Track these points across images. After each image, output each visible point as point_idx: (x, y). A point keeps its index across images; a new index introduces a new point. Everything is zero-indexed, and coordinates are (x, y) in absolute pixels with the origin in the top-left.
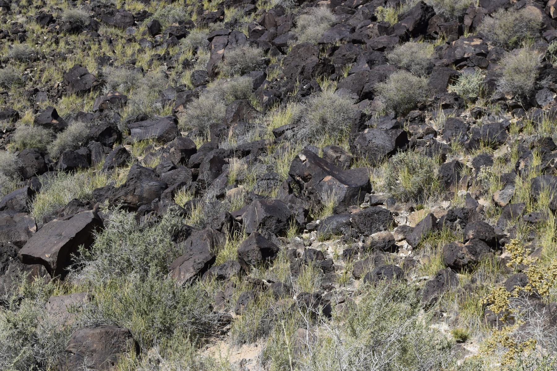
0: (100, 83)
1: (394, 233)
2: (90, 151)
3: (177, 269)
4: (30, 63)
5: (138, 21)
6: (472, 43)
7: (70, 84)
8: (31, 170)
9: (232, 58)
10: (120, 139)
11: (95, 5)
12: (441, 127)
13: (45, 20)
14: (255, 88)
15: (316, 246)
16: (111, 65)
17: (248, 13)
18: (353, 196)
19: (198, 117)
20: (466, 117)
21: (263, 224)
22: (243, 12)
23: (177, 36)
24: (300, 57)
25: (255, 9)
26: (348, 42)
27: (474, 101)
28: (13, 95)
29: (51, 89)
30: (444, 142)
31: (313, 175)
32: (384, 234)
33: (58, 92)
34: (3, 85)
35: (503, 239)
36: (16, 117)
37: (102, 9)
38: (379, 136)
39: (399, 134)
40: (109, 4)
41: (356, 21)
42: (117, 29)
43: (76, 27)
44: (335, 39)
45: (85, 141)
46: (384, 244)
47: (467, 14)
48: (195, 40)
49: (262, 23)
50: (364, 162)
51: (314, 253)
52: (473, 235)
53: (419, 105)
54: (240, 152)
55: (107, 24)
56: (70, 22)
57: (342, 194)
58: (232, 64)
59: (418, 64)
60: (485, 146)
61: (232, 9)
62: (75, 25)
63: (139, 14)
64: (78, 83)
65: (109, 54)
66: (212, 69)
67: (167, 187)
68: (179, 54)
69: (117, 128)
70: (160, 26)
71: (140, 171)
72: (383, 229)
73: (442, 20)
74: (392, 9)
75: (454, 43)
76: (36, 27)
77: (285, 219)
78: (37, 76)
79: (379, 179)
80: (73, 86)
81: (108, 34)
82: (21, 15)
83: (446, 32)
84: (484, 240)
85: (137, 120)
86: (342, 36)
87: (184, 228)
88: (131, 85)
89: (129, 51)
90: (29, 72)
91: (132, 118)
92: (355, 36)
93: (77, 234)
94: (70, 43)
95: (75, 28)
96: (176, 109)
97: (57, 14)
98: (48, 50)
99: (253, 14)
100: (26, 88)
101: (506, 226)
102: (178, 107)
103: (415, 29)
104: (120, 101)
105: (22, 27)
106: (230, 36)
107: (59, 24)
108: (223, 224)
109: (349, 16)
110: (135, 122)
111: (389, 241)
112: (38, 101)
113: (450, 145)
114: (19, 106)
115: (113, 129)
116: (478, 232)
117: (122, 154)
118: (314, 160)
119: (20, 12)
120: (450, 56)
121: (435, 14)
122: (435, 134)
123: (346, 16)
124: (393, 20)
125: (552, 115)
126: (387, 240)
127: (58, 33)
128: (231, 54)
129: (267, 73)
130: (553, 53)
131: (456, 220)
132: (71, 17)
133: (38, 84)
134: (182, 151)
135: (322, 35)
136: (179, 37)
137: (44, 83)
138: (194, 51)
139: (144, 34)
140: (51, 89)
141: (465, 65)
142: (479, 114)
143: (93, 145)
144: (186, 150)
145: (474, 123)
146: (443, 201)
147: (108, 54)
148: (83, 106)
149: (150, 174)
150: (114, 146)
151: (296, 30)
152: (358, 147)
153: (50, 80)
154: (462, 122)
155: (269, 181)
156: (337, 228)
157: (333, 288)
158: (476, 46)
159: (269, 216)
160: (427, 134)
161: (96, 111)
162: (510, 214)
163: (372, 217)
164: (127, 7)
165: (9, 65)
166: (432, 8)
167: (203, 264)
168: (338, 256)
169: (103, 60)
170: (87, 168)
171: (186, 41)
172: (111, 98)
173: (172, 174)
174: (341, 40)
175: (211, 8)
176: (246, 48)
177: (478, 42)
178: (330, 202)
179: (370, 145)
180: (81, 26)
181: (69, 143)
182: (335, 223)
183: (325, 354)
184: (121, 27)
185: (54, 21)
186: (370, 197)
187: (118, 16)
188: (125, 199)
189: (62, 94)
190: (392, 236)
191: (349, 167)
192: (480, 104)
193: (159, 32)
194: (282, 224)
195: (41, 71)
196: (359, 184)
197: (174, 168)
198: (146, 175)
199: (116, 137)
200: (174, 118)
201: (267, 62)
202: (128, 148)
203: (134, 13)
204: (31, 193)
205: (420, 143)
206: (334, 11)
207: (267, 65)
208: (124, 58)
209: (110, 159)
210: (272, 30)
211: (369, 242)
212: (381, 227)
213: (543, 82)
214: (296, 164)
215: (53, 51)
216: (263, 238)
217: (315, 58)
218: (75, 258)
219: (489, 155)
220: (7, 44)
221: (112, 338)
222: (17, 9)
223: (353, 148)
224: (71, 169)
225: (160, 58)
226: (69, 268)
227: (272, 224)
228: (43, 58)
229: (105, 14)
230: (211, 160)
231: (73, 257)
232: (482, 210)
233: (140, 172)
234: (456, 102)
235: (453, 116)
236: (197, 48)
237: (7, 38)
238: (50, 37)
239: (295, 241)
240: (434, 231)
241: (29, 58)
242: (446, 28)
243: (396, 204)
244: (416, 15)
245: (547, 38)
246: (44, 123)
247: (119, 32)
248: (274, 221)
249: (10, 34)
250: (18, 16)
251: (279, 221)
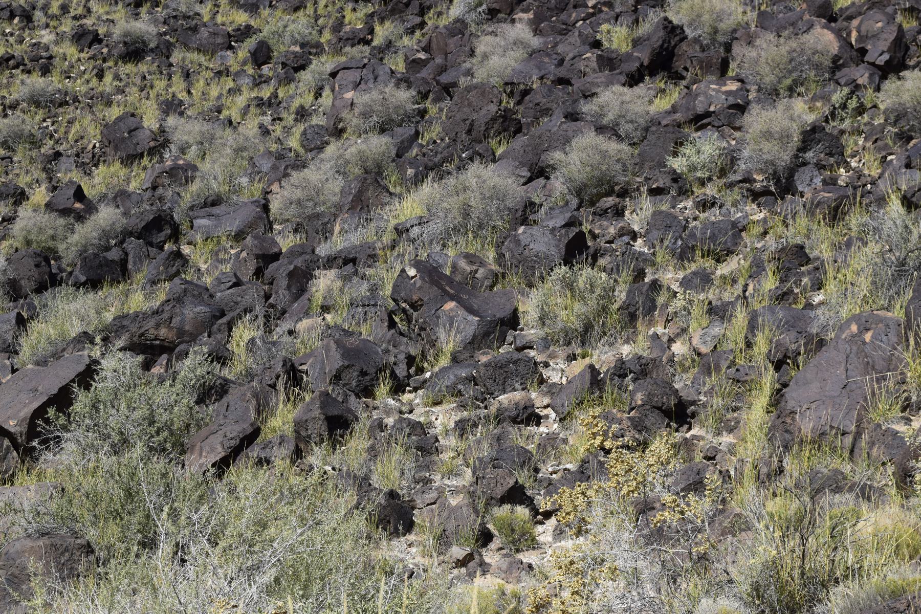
0: (160, 143)
1: (538, 398)
2: (127, 254)
3: (197, 448)
4: (53, 109)
5: (236, 42)
6: (724, 89)
7: (112, 144)
8: (29, 284)
9: (365, 105)
10: (176, 235)
11: (168, 14)
12: (645, 225)
13: (86, 38)
14: (399, 155)
15: (418, 416)
16: (181, 114)
17: (411, 31)
18: (487, 334)
19: (299, 202)
20: (686, 209)
21: (337, 378)
22: (401, 29)
23: (293, 68)
24: (469, 105)
25: (422, 25)
26: (553, 82)
27: (702, 183)
28: (20, 162)
29: (83, 152)
30: (646, 250)
31: (425, 300)
32: (518, 396)
33: (94, 156)
34: (5, 145)
35: (693, 408)
36: (20, 197)
37: (180, 22)
38: (540, 240)
39: (571, 236)
40: (191, 13)
41: (569, 47)
42: (201, 55)
43: (134, 51)
44: (531, 77)
45: (120, 238)
46: (516, 412)
47: (737, 39)
48: (319, 74)
49: (427, 49)
50: (514, 280)
51: (408, 425)
52: (642, 399)
53: (617, 188)
54: (341, 260)
55: (187, 46)
56: (125, 43)
57: (470, 331)
58: (365, 115)
59: (632, 122)
60: (703, 257)
61: (388, 24)
62: (132, 48)
63: (239, 30)
64: (125, 143)
65: (182, 96)
66: (334, 124)
67: (223, 314)
68: (292, 97)
69: (172, 217)
70: (270, 50)
71: (185, 289)
72: (520, 387)
73: (697, 48)
74: (624, 27)
75: (695, 87)
76: (70, 50)
77: (374, 370)
78: (63, 130)
79: (529, 307)
80: (116, 148)
81: (186, 63)
82: (48, 30)
83: (701, 68)
84: (659, 408)
85: (205, 205)
86: (543, 72)
87: (218, 382)
88: (206, 144)
89: (214, 92)
90: (50, 124)
91: (197, 202)
92: (562, 72)
93: (60, 389)
94: (123, 76)
95: (133, 52)
96: (268, 187)
97: (105, 29)
98: (84, 89)
99: (418, 33)
100: (43, 151)
101: (704, 386)
102: (271, 184)
103: (652, 62)
104: (182, 174)
105: (47, 49)
106: (364, 70)
107: (107, 46)
108: (278, 377)
109: (559, 38)
110: (202, 208)
111: (525, 408)
112: (59, 171)
113: (654, 254)
114: (28, 179)
115: (164, 220)
116: (650, 395)
118: (430, 275)
119: (47, 26)
120: (688, 109)
121: (686, 38)
122: (634, 236)
123: (554, 38)
124: (624, 46)
125: (811, 208)
126: (521, 406)
127: (105, 60)
128: (363, 98)
129: (420, 129)
130: (840, 107)
131: (626, 376)
132: (126, 34)
133: (62, 144)
134: (257, 257)
135: (513, 70)
136: (297, 69)
137: (72, 143)
138: (316, 92)
139: (244, 63)
140: (83, 152)
141: (709, 124)
142: (705, 205)
143: (132, 244)
144: (264, 255)
145: (695, 219)
146: (623, 344)
147: (180, 96)
148: (128, 180)
149: (200, 294)
150: (166, 247)
151: (474, 61)
152: (507, 256)
153: (82, 138)
154: (676, 217)
155: (367, 308)
156: (453, 386)
157: (430, 481)
158: (729, 93)
159: (346, 364)
160: (621, 236)
161: (147, 189)
162: (710, 367)
163: (505, 369)
164: (219, 19)
165: (18, 113)
166: (682, 28)
167: (238, 440)
168: (447, 431)
169: (171, 106)
170: (119, 282)
171: (306, 76)
172: (171, 169)
173: (232, 295)
174: (542, 78)
175: (355, 19)
176: (389, 89)
177: (733, 86)
178: (448, 342)
179: (526, 252)
180: (143, 50)
181: (94, 241)
182: (452, 377)
184: (208, 52)
185: (100, 41)
186: (515, 337)
187: (204, 33)
188: (156, 333)
189: (99, 160)
190: (530, 400)
191: (491, 287)
192: (710, 191)
193: (267, 59)
194: (368, 378)
195: (69, 122)
196: (498, 316)
197: (238, 284)
198: (194, 296)
199: (169, 231)
200: (264, 202)
201: (422, 113)
202: (186, 250)
203: (230, 29)
204: (21, 322)
205: (606, 250)
206: (537, 31)
207: (422, 117)
208: (204, 103)
209: (155, 268)
210: (439, 60)
211: (493, 409)
212: (517, 386)
213: (809, 155)
214: (401, 282)
215: (92, 89)
216: (335, 400)
217: (493, 108)
218: (44, 428)
219: (709, 270)
220: (20, 77)
221: (62, 554)
222: (44, 20)
223: (500, 257)
224: (94, 284)
225: (261, 103)
226: (34, 444)
227: (352, 378)
228: (74, 102)
229: (184, 29)
230: (290, 272)
231: (40, 425)
232: (671, 360)
233: (185, 291)
234: (675, 185)
235: (663, 208)
236: (321, 88)
237: (21, 68)
238: (91, 67)
239: (386, 405)
240: (593, 393)
241: (51, 102)
242: (701, 62)
243: (551, 348)
244: (655, 40)
245: (840, 81)
246: (61, 207)
247: (202, 59)
248: (356, 374)
249: (27, 61)
250: (43, 32)
251: (363, 373)
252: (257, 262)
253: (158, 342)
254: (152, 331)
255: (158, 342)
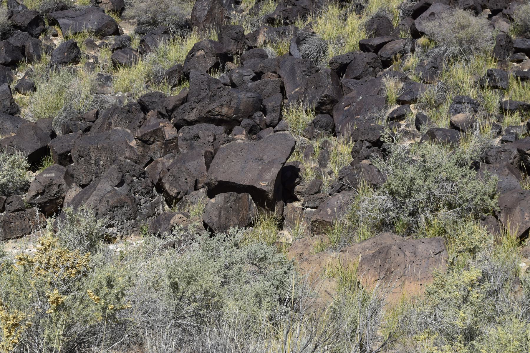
117: (73, 49)
144: (221, 54)
183: (483, 306)
252: (217, 59)
253: (219, 117)
254: (217, 109)
255: (219, 117)
